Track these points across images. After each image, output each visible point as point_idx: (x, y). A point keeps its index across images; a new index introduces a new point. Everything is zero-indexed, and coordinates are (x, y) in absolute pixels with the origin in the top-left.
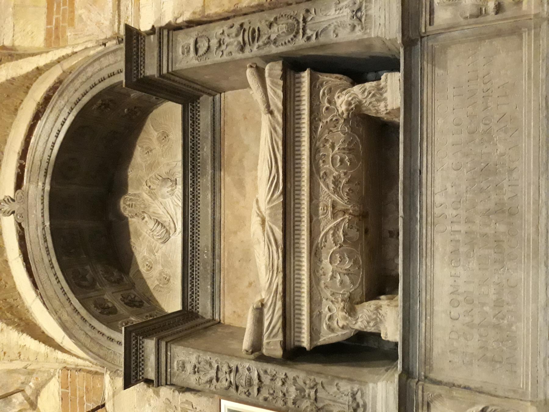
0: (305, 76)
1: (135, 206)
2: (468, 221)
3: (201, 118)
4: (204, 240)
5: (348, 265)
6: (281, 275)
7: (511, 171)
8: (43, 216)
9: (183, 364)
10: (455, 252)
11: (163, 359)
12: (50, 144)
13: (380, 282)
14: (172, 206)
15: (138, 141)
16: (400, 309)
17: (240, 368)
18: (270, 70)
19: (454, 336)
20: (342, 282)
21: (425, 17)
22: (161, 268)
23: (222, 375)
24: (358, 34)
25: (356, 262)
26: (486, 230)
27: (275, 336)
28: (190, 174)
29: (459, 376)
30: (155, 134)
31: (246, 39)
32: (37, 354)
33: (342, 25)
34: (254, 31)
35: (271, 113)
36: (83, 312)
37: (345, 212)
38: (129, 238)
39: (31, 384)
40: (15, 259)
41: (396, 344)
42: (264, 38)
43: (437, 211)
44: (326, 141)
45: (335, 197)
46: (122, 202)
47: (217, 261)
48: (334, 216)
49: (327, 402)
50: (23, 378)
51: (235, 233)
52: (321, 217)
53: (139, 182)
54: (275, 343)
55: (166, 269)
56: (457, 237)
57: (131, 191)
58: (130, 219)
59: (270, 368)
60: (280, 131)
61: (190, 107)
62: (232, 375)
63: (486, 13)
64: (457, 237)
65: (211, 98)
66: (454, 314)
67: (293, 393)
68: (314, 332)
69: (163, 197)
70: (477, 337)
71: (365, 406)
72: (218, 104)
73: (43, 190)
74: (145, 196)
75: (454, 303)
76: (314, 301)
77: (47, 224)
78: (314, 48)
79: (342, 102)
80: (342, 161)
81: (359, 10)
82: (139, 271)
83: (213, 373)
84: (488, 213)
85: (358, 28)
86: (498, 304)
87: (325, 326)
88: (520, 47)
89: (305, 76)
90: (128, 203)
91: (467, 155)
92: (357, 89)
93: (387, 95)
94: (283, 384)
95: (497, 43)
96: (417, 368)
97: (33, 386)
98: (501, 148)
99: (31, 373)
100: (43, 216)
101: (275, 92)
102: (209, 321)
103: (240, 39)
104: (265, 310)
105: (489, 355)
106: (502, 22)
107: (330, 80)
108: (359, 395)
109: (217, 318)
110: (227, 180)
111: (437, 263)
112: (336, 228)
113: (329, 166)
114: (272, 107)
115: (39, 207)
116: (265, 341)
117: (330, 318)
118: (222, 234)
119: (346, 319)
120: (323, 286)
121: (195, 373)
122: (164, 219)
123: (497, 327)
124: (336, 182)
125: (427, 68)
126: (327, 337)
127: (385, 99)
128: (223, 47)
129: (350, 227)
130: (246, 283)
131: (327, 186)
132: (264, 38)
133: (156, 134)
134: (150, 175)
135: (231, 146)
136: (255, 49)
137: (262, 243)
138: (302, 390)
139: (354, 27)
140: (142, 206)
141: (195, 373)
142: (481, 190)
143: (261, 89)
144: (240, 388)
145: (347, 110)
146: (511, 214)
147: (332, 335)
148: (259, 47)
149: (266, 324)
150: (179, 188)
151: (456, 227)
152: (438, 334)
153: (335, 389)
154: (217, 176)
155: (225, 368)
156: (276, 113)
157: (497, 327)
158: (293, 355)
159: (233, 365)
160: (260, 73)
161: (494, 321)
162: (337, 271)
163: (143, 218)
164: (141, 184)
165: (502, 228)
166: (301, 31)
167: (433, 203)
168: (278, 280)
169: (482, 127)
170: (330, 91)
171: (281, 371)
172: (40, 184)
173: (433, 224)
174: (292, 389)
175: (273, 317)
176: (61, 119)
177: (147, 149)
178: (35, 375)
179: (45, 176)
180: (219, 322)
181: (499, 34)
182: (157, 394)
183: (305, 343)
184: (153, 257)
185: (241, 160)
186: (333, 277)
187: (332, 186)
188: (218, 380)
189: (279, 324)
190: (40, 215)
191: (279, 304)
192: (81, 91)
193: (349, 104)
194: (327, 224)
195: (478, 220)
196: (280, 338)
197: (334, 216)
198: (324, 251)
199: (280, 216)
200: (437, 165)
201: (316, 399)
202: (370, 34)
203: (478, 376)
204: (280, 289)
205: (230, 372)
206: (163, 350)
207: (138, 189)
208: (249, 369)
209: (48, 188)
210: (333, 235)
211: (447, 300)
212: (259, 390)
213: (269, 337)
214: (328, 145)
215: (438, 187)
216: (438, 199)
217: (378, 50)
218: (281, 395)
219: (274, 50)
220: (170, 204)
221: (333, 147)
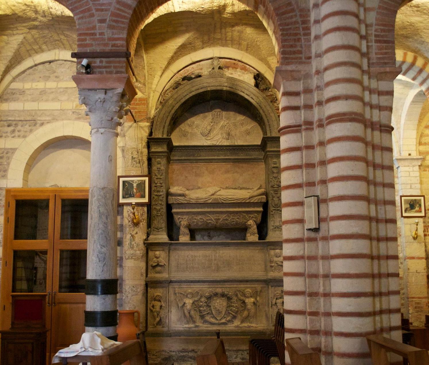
0: (261, 209)
1: (217, 118)
2: (215, 260)
3: (255, 152)
4: (204, 156)
5: (200, 223)
6: (195, 202)
7: (229, 270)
8: (212, 86)
9: (160, 163)
10: (206, 256)
11: (160, 154)
12: (243, 90)
13: (193, 233)
14: (217, 138)
15: (247, 118)
16: (188, 242)
17: (162, 187)
18: (264, 198)
19: (183, 256)
20: (194, 222)
21: (272, 247)
22: (190, 132)
23: (158, 180)
24: (272, 228)
25: (201, 226)
26: (213, 264)
27: (175, 201)
28: (231, 148)
29: (172, 258)
30: (249, 127)
31: (275, 188)
32: (152, 84)
33: (274, 223)
34: (277, 191)
35: (249, 198)
36: (173, 111)
37: (217, 222)
38: (202, 113)
39: (140, 85)
40: (191, 59)
41: (178, 240)
42: (274, 195)
43: (218, 251)
44: (240, 216)
45: (221, 219)
46: (219, 110)
47: (195, 162)
48: (215, 219)
49: (157, 219)
50: (142, 81)
51: (207, 170)
52: (215, 215)
53: (228, 118)
54: (173, 201)
55: (189, 134)
56: (211, 257)
57: (224, 113)
58: (211, 113)
59: (165, 199)
60: (243, 201)
61: (259, 148)
62: (160, 185)
63: (271, 263)
64: (211, 257)
65: (262, 157)
66: (189, 256)
67: (158, 208)
68: (178, 213)
69: (222, 134)
70: (184, 262)
71: (159, 232)
72: (260, 161)
73: (224, 86)
74: (222, 123)
75: (192, 256)
76: (188, 213)
77: (209, 89)
78: (270, 213)
79: (251, 222)
80: (233, 221)
81: (278, 228)
82: (187, 119)
83: (159, 177)
84: (217, 265)
85: (273, 228)
86: (193, 268)
87: (179, 216)
88: (262, 272)
89: (261, 209)
90: (218, 113)
91: (233, 259)
92: (255, 226)
93: (252, 237)
94: (160, 204)
95: (263, 266)
96: (172, 247)
97: (139, 86)
98: (235, 267)
99: (144, 84)
100: (212, 86)
101: (255, 200)
102: (170, 158)
103: (275, 186)
104: (183, 197)
105: (179, 266)
106: (268, 267)
107: (259, 217)
108: (161, 230)
109: (172, 162)
110: (229, 166)
111: (203, 252)
112: (211, 220)
113: (232, 217)
114: (251, 199)
115: (217, 84)
116: (174, 197)
117: (182, 218)
118: (206, 164)
119: (184, 225)
120: (192, 216)
121: (158, 168)
122: (211, 134)
123: (187, 267)
124: (227, 220)
125: (259, 248)
126: (176, 217)
127: (251, 236)
128: (274, 179)
129: (212, 224)
130: (187, 175)
131: (225, 217)
132: (274, 195)
133: (249, 128)
134: (231, 125)
135: (242, 167)
136: (271, 192)
137: (206, 195)
138: (159, 211)
139: (273, 226)
140: (217, 122)
141: (158, 168)
142: (224, 263)
143: (257, 194)
144: (156, 188)
145: (248, 225)
146: (217, 271)
147: (177, 219)
148: (272, 193)
149: (179, 198)
150: (226, 143)
151: (213, 256)
152: (183, 252)
153: (162, 222)
154: (230, 161)
155: (161, 182)
156: (249, 200)
157: (187, 267)
158: (169, 207)
159: (163, 185)
160: (262, 194)
161: (188, 267)
162: (198, 220)
163: (212, 123)
164: (227, 119)
165: (213, 268)
166: (274, 209)
167: (220, 250)
168: (193, 201)
169: (241, 263)
170: (256, 217)
171: (164, 203)
172: (226, 84)
173: (214, 250)
174: (159, 208)
175: (181, 199)
176: (254, 98)
177: (243, 123)
178: (143, 86)
179: (229, 87)
180: (169, 163)
181: (266, 266)
182: (144, 148)
183: (174, 210)
184: (194, 127)
185: (237, 172)
186: (195, 219)
187: (225, 218)
188: (157, 178)
189: (180, 202)
190: (213, 85)
191: (186, 202)
192: (265, 109)
193: (250, 225)
194: (213, 217)
195: (216, 262)
196: (175, 202)
197: (215, 219)
198: (204, 216)
199: (215, 202)
200: (230, 251)
201: (157, 216)
202: (271, 231)
203: (173, 263)
204: (191, 202)
205: (160, 184)
206: (164, 154)
207: (225, 118)
208: (163, 191)
209: (225, 89)
210: (209, 219)
211: (193, 254)
212: (156, 195)
213: (175, 199)
214: (238, 217)
215: (224, 251)
216: (221, 252)
217: (266, 234)
218: (157, 203)
219: (270, 199)
220: (217, 139)
221: (238, 218)
